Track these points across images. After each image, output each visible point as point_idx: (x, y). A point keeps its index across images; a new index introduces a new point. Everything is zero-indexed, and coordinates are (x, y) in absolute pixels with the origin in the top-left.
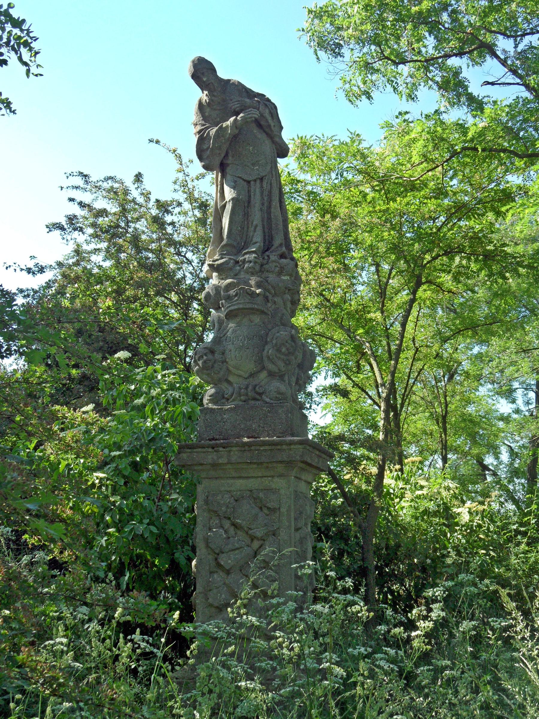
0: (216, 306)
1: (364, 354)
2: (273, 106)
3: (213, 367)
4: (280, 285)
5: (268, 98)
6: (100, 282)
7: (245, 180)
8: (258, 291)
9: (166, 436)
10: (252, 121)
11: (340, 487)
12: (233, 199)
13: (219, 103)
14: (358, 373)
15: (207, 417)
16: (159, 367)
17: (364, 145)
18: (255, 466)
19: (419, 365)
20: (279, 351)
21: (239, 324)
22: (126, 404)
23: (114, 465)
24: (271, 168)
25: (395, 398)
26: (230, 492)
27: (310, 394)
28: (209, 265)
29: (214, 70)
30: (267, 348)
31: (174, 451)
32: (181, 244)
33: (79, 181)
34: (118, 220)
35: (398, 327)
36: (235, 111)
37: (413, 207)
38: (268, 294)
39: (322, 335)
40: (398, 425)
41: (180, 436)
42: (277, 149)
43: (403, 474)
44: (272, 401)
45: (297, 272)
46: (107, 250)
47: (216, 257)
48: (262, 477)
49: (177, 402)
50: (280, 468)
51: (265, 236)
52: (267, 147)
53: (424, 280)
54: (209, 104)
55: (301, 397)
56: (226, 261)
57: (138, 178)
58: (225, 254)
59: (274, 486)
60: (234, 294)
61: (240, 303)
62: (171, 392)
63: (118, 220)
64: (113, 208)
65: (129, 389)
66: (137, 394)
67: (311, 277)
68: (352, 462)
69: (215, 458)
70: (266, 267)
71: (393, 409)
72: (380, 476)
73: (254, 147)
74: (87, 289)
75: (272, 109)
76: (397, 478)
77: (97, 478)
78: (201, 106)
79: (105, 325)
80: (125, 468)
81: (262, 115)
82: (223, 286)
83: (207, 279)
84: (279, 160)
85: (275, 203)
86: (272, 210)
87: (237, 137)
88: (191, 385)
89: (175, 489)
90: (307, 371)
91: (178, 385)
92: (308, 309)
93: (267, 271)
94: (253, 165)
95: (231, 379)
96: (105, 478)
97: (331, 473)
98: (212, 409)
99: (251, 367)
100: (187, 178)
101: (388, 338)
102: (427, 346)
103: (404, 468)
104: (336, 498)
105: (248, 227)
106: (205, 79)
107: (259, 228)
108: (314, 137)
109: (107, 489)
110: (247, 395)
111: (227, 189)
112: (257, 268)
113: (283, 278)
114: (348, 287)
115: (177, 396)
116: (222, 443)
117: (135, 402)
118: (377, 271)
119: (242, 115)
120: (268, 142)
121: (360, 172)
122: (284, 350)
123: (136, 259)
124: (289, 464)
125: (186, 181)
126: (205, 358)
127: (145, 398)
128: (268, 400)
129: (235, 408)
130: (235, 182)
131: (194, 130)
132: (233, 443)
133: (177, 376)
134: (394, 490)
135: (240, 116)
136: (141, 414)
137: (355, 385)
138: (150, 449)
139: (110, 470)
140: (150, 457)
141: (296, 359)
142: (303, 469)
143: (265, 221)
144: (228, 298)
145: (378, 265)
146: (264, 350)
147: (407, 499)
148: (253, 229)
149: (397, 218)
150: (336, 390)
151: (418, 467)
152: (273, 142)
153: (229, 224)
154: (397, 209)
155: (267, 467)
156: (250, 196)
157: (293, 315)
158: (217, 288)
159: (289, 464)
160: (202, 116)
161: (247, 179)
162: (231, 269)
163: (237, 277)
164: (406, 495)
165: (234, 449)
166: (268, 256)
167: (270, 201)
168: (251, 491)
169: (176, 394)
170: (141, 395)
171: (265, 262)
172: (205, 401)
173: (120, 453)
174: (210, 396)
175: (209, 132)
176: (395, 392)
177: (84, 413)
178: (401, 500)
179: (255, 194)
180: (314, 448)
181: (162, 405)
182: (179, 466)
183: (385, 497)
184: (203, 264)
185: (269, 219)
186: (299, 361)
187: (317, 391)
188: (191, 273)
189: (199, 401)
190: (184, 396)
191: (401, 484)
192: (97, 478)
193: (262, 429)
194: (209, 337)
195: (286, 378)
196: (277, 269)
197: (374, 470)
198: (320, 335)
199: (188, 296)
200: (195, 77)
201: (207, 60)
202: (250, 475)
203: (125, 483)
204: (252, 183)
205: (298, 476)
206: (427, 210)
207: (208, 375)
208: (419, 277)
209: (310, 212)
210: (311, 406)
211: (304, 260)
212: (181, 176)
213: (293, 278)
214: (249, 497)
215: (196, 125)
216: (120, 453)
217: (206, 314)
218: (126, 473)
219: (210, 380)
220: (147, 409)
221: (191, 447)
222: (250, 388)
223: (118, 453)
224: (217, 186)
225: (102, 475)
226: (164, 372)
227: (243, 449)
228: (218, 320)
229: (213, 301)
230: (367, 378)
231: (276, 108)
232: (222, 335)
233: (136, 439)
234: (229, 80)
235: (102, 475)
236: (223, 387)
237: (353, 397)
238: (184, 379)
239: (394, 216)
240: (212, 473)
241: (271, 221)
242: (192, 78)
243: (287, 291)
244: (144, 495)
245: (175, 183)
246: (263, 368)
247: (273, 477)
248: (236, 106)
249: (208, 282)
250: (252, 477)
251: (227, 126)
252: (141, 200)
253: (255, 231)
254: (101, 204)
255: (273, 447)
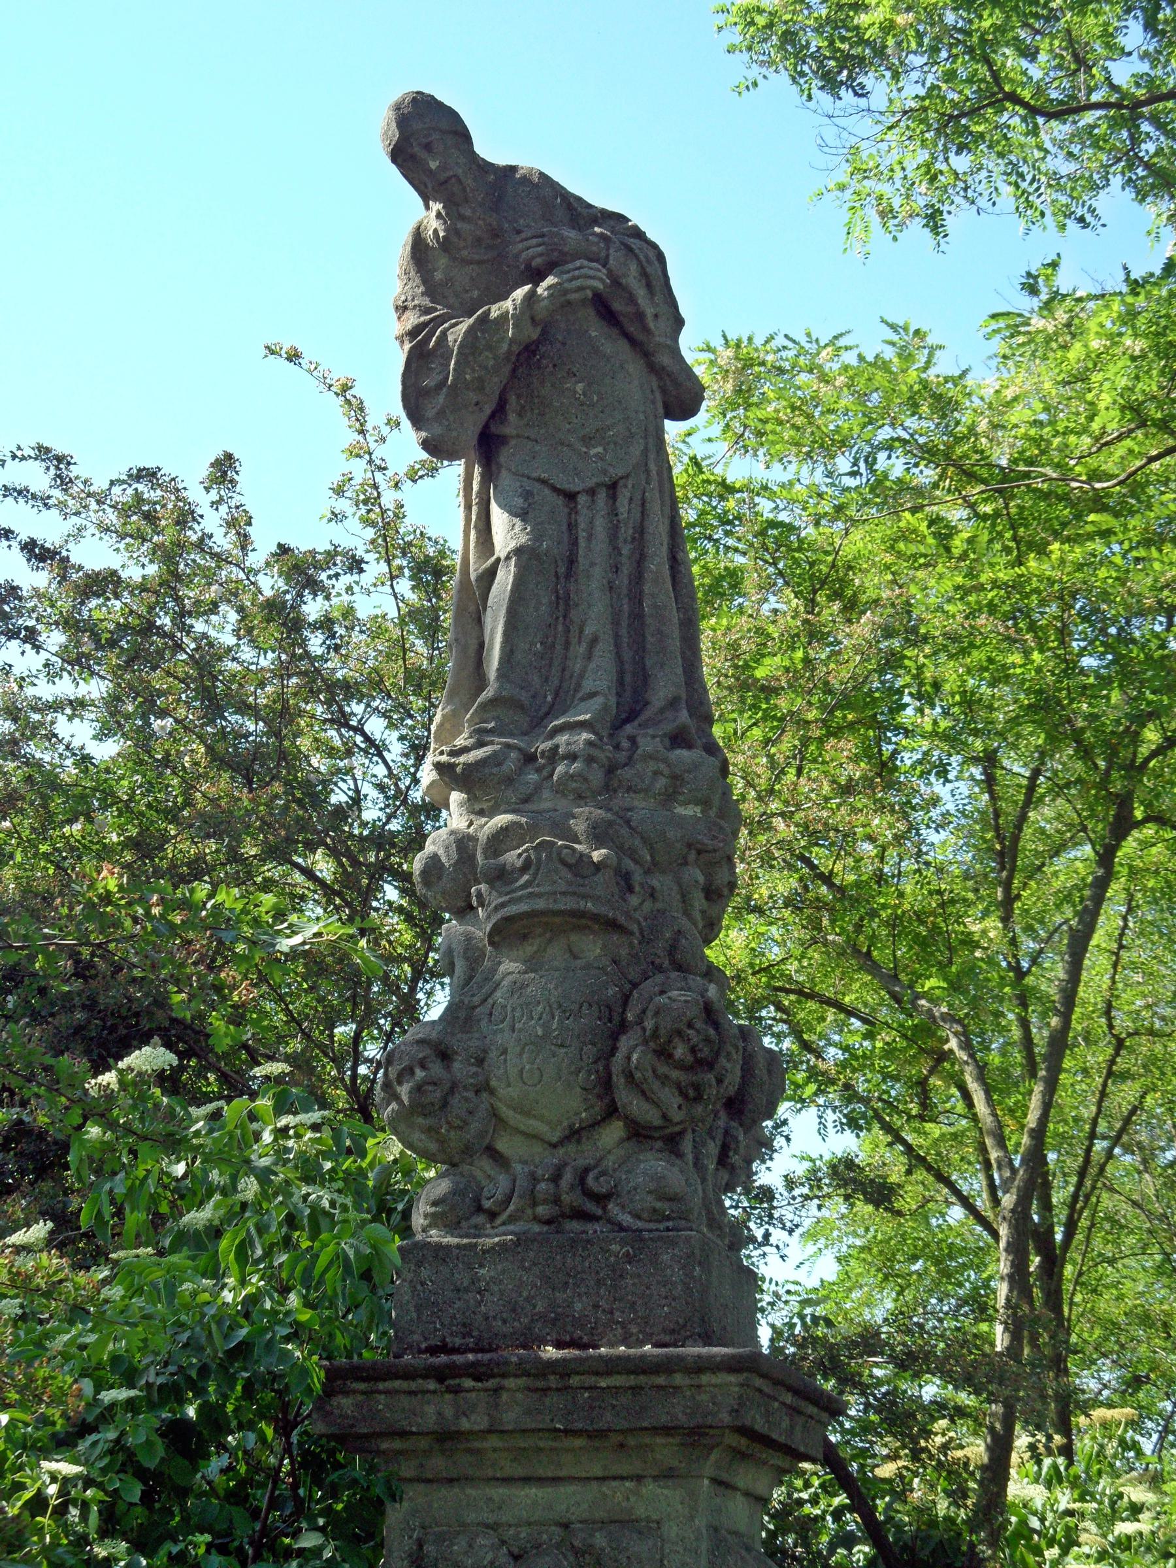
0: (461, 904)
1: (943, 1056)
2: (652, 254)
3: (445, 1104)
4: (671, 834)
5: (636, 228)
6: (81, 809)
7: (555, 489)
8: (597, 855)
9: (287, 1339)
10: (584, 301)
11: (861, 1503)
12: (518, 551)
13: (479, 240)
14: (922, 1118)
15: (425, 1273)
16: (264, 1103)
17: (945, 366)
18: (579, 1442)
19: (1125, 1095)
20: (664, 1053)
21: (533, 964)
22: (157, 1221)
23: (112, 1435)
24: (645, 451)
25: (1047, 1206)
26: (494, 1527)
27: (767, 1194)
28: (438, 766)
29: (462, 135)
30: (624, 1043)
31: (309, 1390)
32: (350, 689)
33: (37, 477)
34: (151, 609)
35: (1055, 968)
36: (528, 267)
37: (1102, 573)
38: (629, 864)
39: (803, 994)
40: (1054, 1298)
41: (331, 1336)
42: (664, 391)
43: (1070, 1463)
44: (640, 1224)
45: (727, 790)
46: (113, 702)
47: (460, 742)
48: (603, 1479)
49: (324, 1223)
50: (666, 1451)
51: (621, 673)
52: (633, 384)
53: (1139, 814)
54: (445, 244)
55: (733, 1204)
56: (495, 754)
57: (224, 470)
58: (490, 732)
59: (641, 1511)
60: (519, 863)
61: (539, 895)
62: (305, 1190)
63: (151, 609)
64: (138, 569)
65: (169, 1175)
66: (189, 1193)
67: (775, 806)
68: (902, 1420)
69: (449, 1412)
70: (625, 773)
71: (1040, 1249)
72: (997, 1469)
73: (589, 385)
74: (41, 832)
75: (651, 263)
76: (1054, 1480)
77: (54, 1479)
78: (419, 249)
79: (93, 955)
80: (149, 1443)
81: (616, 282)
82: (483, 835)
83: (433, 809)
84: (668, 424)
85: (657, 564)
86: (647, 588)
87: (531, 356)
88: (371, 1165)
89: (312, 1519)
90: (756, 1122)
91: (328, 1165)
92: (759, 910)
93: (629, 789)
94: (587, 440)
95: (502, 1145)
96: (78, 1477)
97: (831, 1458)
98: (439, 1246)
99: (569, 1103)
100: (379, 476)
101: (1024, 1005)
102: (1152, 1032)
103: (1077, 1445)
104: (848, 1541)
105: (567, 644)
106: (433, 165)
107: (604, 649)
108: (780, 341)
109: (84, 1517)
110: (557, 1201)
111: (499, 518)
112: (597, 777)
113: (680, 810)
114: (898, 839)
115: (326, 1204)
116: (473, 1364)
117: (186, 1219)
118: (990, 782)
119: (550, 280)
120: (635, 367)
121: (929, 453)
122: (680, 1051)
123: (201, 738)
124: (696, 1436)
125: (375, 487)
126: (420, 1074)
127: (217, 1207)
128: (626, 1219)
129: (517, 1243)
130: (527, 495)
131: (397, 327)
132: (507, 1363)
133: (326, 1133)
134: (1042, 1520)
135: (545, 284)
136: (202, 1261)
137: (916, 1160)
138: (232, 1381)
139: (98, 1451)
140: (230, 1408)
141: (720, 1081)
142: (741, 1456)
143: (624, 623)
144: (501, 877)
145: (990, 760)
146: (613, 1050)
147: (1086, 1549)
148: (582, 650)
149: (1053, 609)
150: (847, 1177)
151: (1122, 1442)
152: (654, 369)
153: (506, 634)
154: (1051, 582)
155: (622, 1445)
156: (574, 543)
157: (711, 929)
158: (463, 843)
159: (696, 1436)
160: (425, 282)
161: (566, 486)
162: (509, 781)
163: (529, 807)
164: (1083, 1537)
165: (510, 1383)
166: (633, 740)
167: (640, 560)
168: (566, 1526)
169: (323, 1197)
170: (210, 1195)
171: (622, 756)
172: (418, 1220)
173: (133, 1393)
174: (435, 1204)
175: (444, 334)
176: (1047, 1187)
177: (19, 1249)
178: (1065, 1551)
179: (590, 538)
180: (777, 1383)
181: (275, 1232)
182: (330, 1437)
183: (1012, 1542)
184: (419, 760)
185: (637, 616)
186: (732, 1091)
187: (790, 1184)
188: (381, 788)
189: (396, 1218)
190: (349, 1201)
191: (1065, 1499)
192: (54, 1479)
193: (603, 1318)
194: (436, 1003)
195: (687, 1146)
196: (661, 782)
197: (976, 1450)
198: (800, 992)
199: (368, 865)
200: (401, 155)
201: (440, 105)
202: (563, 1473)
203: (147, 1498)
204: (582, 499)
205: (725, 1476)
206: (1149, 581)
207: (430, 1131)
208: (1124, 803)
209: (767, 586)
210: (767, 1235)
211: (745, 745)
212: (359, 469)
213: (712, 813)
214: (558, 1546)
215: (402, 309)
216: (133, 1393)
217: (425, 922)
218: (151, 1463)
219: (433, 1147)
220: (224, 1243)
221: (372, 1374)
222: (568, 1177)
223: (123, 1394)
224: (468, 507)
225: (68, 1469)
226: (283, 1121)
227: (541, 1384)
228: (466, 950)
229: (444, 891)
230: (955, 1136)
231: (661, 257)
232: (476, 1000)
233: (186, 1346)
234: (513, 169)
235: (68, 1469)
236: (479, 1174)
237: (908, 1201)
238: (348, 1142)
239: (1043, 603)
240: (438, 1464)
241: (643, 624)
242: (394, 161)
243: (692, 856)
244: (207, 1538)
245: (339, 491)
246: (612, 1111)
247: (639, 1478)
248: (533, 252)
249: (437, 818)
250: (572, 1479)
251: (504, 317)
252: (223, 541)
253: (589, 657)
254: (95, 554)
255: (642, 1379)
